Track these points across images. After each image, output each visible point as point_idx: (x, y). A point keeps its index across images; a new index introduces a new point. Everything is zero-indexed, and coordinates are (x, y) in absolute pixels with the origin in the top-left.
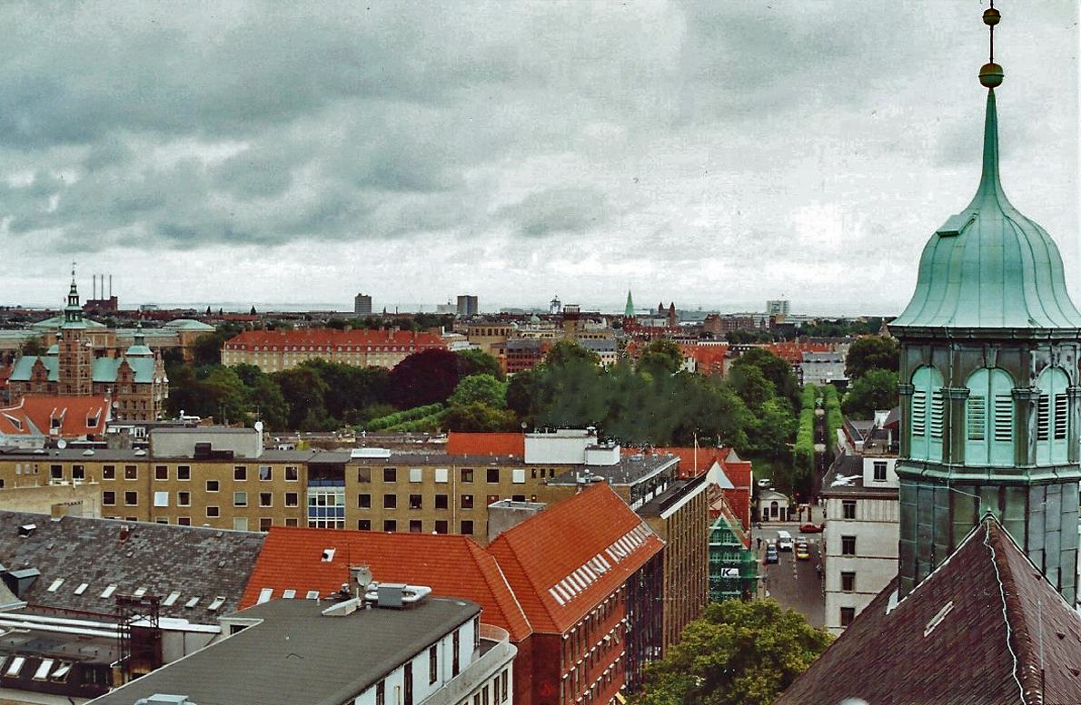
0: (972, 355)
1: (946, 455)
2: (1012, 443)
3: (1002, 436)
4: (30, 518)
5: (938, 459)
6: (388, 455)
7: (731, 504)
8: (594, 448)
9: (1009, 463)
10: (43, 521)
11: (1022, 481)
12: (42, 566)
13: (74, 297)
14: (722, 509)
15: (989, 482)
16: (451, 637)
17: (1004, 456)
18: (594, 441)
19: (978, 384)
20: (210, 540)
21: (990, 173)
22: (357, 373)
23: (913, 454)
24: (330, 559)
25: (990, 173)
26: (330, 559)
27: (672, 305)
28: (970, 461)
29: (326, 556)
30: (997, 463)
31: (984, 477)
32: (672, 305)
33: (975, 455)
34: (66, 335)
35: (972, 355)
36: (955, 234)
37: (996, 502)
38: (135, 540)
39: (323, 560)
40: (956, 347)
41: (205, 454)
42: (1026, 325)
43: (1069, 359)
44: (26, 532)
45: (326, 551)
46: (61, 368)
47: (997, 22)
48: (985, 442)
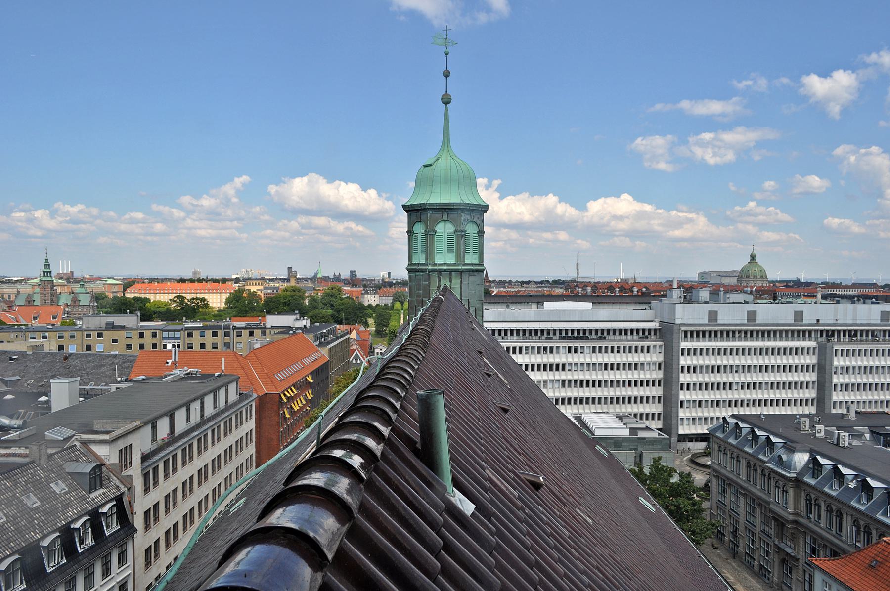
0: (437, 215)
1: (427, 259)
2: (454, 253)
3: (450, 250)
4: (14, 353)
5: (423, 261)
6: (201, 325)
7: (359, 345)
8: (297, 319)
9: (453, 262)
10: (23, 354)
11: (459, 269)
12: (21, 375)
13: (47, 272)
14: (357, 349)
15: (445, 270)
16: (224, 389)
17: (451, 259)
18: (298, 316)
19: (440, 228)
20: (110, 358)
21: (446, 141)
22: (273, 463)
23: (413, 261)
24: (169, 364)
25: (446, 141)
26: (169, 364)
27: (340, 274)
28: (438, 261)
29: (167, 363)
30: (448, 262)
31: (443, 268)
32: (340, 274)
33: (439, 259)
34: (43, 283)
35: (437, 215)
36: (430, 165)
37: (448, 279)
38: (71, 360)
39: (166, 365)
40: (430, 212)
41: (111, 326)
42: (459, 201)
43: (478, 219)
44: (12, 359)
45: (168, 361)
46: (41, 299)
47: (449, 76)
48: (443, 253)
